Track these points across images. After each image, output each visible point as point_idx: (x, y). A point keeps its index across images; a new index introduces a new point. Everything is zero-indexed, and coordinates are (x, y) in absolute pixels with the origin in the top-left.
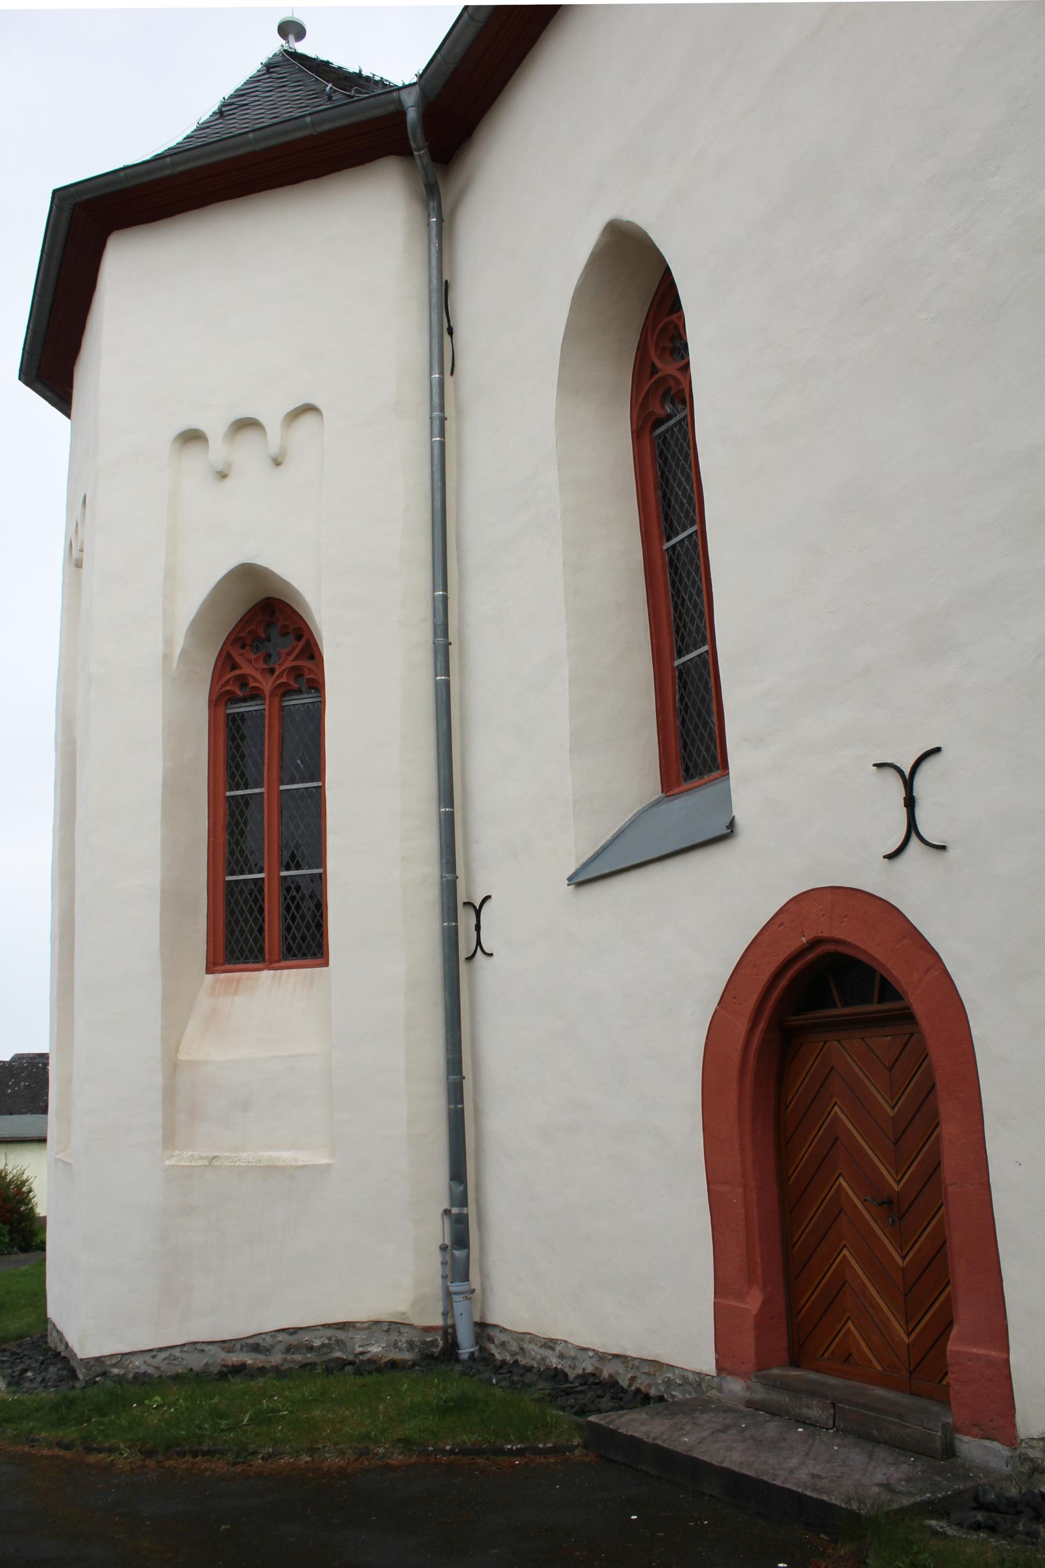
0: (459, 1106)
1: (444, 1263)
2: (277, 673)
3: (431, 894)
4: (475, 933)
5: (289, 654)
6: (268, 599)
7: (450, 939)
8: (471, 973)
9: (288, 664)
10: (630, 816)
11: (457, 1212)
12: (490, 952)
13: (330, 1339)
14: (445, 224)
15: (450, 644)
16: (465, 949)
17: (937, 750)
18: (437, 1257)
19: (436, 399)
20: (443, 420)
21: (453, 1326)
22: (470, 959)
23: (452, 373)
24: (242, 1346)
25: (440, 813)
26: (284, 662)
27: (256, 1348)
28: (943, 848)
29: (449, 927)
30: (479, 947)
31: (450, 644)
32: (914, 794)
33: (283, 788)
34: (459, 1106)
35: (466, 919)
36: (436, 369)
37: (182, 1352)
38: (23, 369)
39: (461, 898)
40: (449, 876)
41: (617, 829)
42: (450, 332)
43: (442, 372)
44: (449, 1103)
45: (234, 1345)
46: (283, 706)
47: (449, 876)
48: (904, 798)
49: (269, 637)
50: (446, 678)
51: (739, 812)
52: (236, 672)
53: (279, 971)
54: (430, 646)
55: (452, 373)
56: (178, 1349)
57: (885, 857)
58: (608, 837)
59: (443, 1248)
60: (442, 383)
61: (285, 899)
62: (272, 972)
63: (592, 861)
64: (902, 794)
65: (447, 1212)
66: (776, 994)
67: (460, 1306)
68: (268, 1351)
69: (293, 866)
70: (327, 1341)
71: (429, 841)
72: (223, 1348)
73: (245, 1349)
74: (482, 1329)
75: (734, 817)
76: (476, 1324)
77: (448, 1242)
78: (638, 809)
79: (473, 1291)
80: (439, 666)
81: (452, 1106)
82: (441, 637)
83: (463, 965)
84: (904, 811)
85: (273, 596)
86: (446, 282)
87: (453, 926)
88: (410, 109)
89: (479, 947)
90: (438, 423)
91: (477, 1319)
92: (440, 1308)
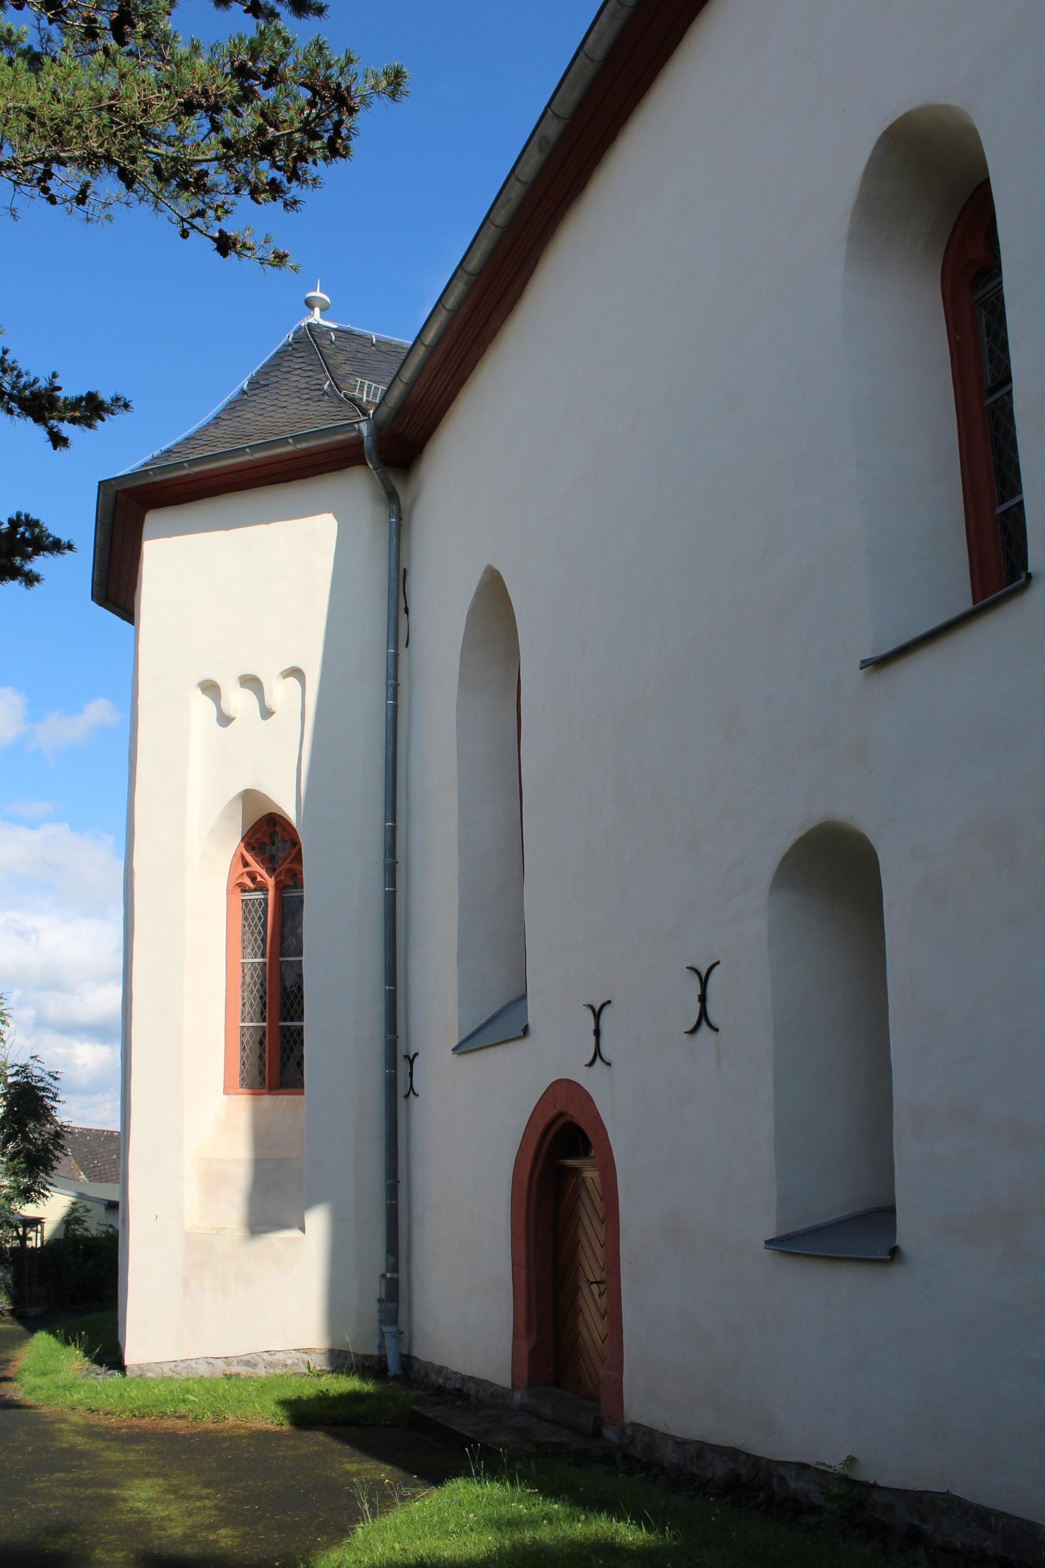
0: (394, 1202)
1: (380, 1311)
2: (277, 871)
3: (376, 1049)
4: (409, 1079)
5: (286, 858)
6: (271, 813)
7: (391, 1084)
8: (408, 1108)
9: (286, 865)
10: (500, 1007)
11: (390, 1276)
12: (417, 1093)
13: (298, 1359)
14: (404, 522)
15: (397, 863)
16: (402, 1088)
17: (609, 1002)
18: (375, 1307)
19: (391, 670)
20: (396, 687)
21: (385, 1356)
22: (407, 1096)
23: (407, 646)
24: (238, 1362)
25: (386, 990)
26: (283, 863)
27: (247, 1363)
28: (609, 1064)
29: (389, 1073)
30: (703, 978)
31: (397, 863)
32: (600, 1028)
33: (282, 959)
34: (394, 1202)
35: (402, 1066)
36: (392, 645)
37: (196, 1363)
38: (94, 594)
39: (401, 1051)
40: (391, 1037)
41: (490, 1016)
42: (407, 611)
43: (396, 648)
44: (387, 1200)
45: (233, 1361)
46: (283, 897)
47: (391, 1037)
48: (699, 995)
49: (274, 841)
50: (393, 889)
51: (531, 1021)
52: (248, 869)
53: (276, 1096)
54: (382, 864)
55: (407, 646)
56: (194, 1361)
57: (586, 1066)
58: (483, 1022)
59: (380, 1301)
60: (396, 656)
61: (283, 1042)
62: (271, 1096)
63: (471, 1038)
64: (593, 1027)
65: (383, 1276)
66: (550, 1137)
67: (389, 1342)
68: (255, 1366)
69: (288, 1018)
70: (296, 1361)
71: (377, 1009)
72: (225, 1363)
73: (240, 1364)
74: (407, 1361)
75: (528, 1024)
76: (402, 1356)
77: (383, 1297)
78: (506, 1002)
79: (402, 1333)
80: (387, 880)
81: (388, 1202)
82: (389, 858)
83: (401, 1101)
84: (593, 1038)
85: (275, 812)
86: (405, 569)
87: (393, 1073)
88: (405, 381)
89: (703, 978)
90: (392, 690)
91: (405, 1352)
92: (377, 1342)
